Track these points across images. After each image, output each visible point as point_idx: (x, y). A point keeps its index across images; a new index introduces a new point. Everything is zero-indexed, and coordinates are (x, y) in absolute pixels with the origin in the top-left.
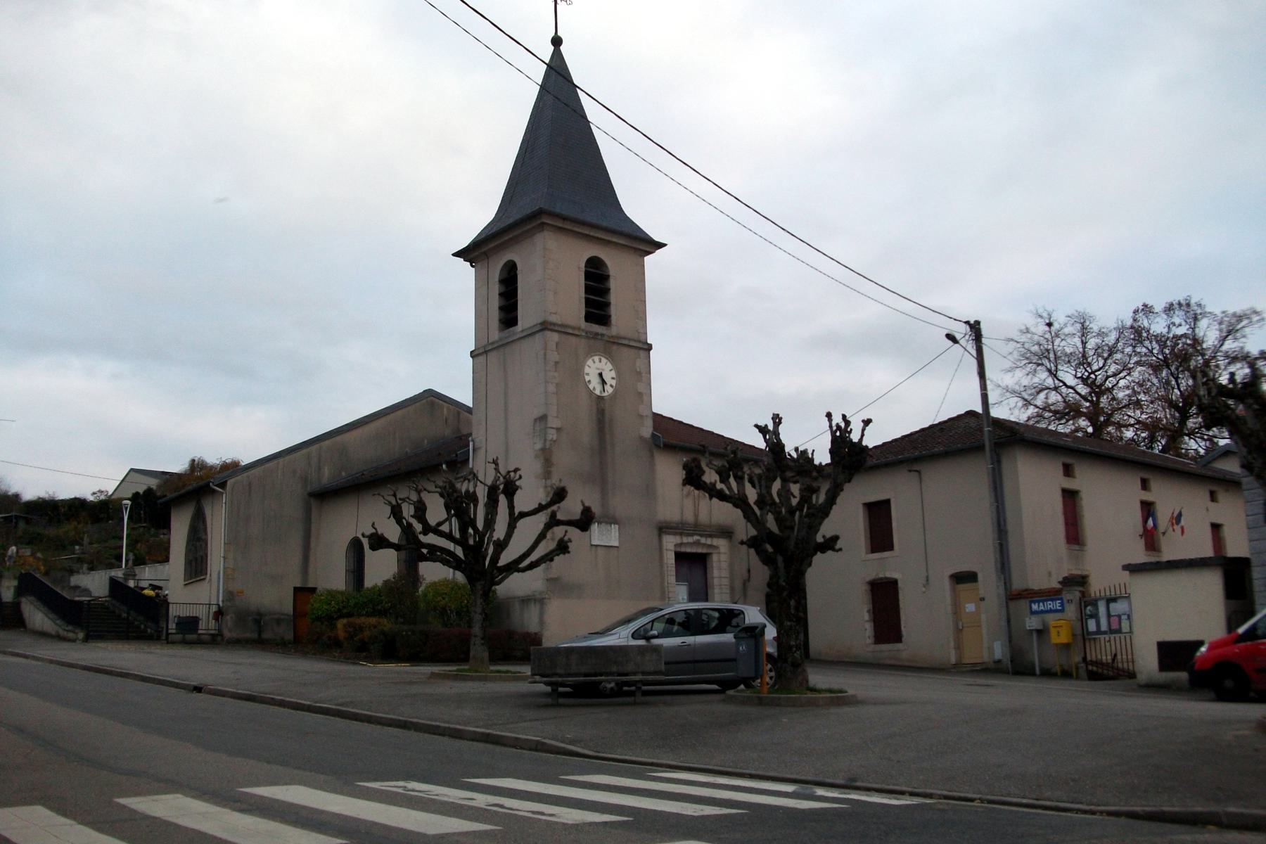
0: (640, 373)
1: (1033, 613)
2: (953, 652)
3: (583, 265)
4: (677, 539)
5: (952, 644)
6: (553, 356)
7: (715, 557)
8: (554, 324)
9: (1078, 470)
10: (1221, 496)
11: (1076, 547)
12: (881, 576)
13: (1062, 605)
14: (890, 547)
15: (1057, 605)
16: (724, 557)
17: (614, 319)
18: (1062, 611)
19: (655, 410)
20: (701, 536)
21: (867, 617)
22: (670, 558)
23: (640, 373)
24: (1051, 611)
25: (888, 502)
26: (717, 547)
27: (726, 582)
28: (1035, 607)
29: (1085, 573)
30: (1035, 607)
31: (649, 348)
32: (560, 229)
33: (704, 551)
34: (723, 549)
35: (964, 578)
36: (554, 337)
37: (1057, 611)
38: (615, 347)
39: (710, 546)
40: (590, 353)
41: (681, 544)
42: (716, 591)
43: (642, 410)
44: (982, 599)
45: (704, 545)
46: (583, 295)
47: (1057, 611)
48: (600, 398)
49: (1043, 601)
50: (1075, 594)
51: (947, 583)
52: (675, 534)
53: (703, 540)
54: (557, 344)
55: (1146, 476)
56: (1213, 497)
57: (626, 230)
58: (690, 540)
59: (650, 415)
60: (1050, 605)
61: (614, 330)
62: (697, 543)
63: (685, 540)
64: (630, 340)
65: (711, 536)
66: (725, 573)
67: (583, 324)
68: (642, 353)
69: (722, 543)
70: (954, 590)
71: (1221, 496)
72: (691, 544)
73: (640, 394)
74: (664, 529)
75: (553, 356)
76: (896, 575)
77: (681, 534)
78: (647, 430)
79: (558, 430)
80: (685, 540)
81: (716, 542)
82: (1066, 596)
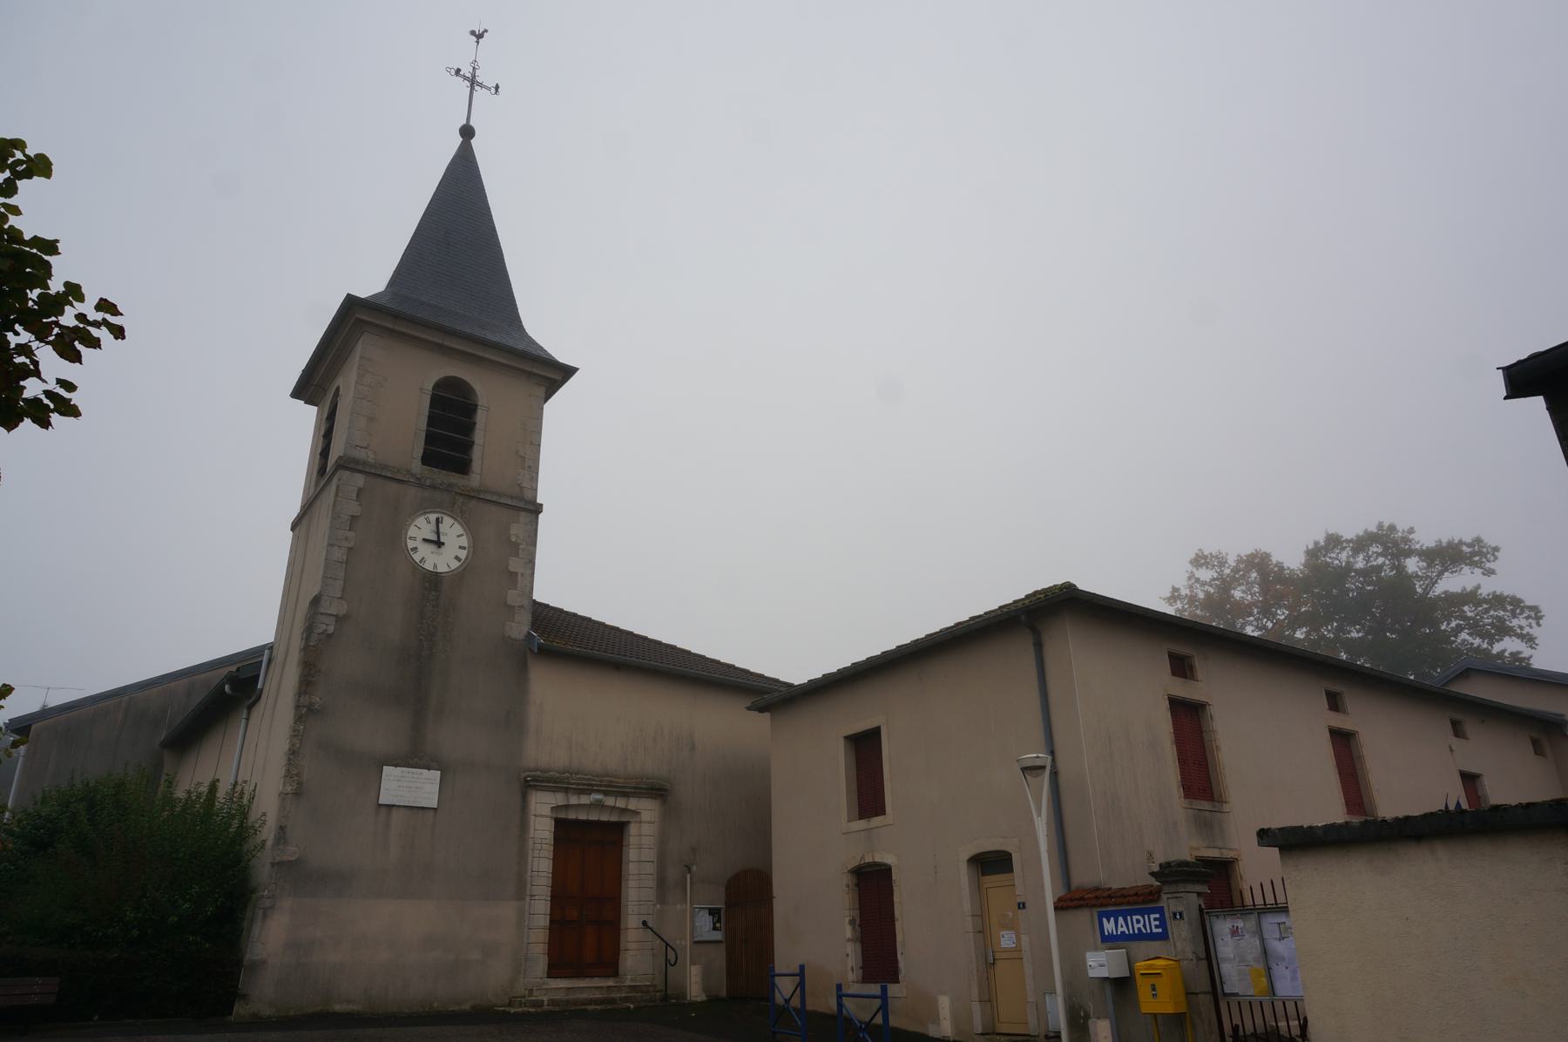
0: (515, 545)
1: (1109, 940)
2: (976, 1008)
3: (429, 386)
4: (560, 799)
5: (975, 992)
6: (354, 508)
7: (633, 829)
8: (365, 463)
9: (1201, 666)
10: (1470, 727)
11: (1206, 805)
12: (868, 859)
13: (1163, 924)
14: (880, 810)
15: (1151, 923)
16: (647, 829)
17: (476, 465)
18: (1164, 936)
19: (542, 594)
20: (606, 793)
21: (849, 932)
22: (542, 830)
23: (515, 545)
24: (1140, 937)
25: (878, 728)
26: (636, 813)
27: (650, 868)
28: (1109, 926)
29: (1228, 854)
30: (1109, 926)
31: (537, 509)
32: (391, 332)
33: (614, 818)
34: (645, 816)
35: (992, 864)
36: (360, 480)
37: (1152, 937)
38: (473, 503)
39: (624, 811)
40: (422, 508)
41: (567, 807)
42: (632, 884)
43: (513, 597)
44: (1022, 906)
45: (613, 808)
46: (424, 426)
47: (1152, 937)
48: (433, 580)
49: (1125, 914)
50: (1187, 900)
51: (964, 874)
52: (554, 790)
53: (610, 801)
54: (360, 491)
55: (1337, 688)
56: (1458, 730)
57: (521, 346)
58: (585, 800)
59: (526, 603)
60: (1138, 923)
61: (474, 480)
62: (599, 805)
63: (574, 800)
64: (500, 495)
65: (625, 795)
66: (650, 854)
67: (416, 466)
68: (523, 517)
69: (648, 809)
70: (979, 892)
71: (1470, 727)
72: (584, 808)
73: (513, 576)
74: (534, 782)
75: (354, 508)
76: (888, 859)
77: (566, 790)
78: (520, 627)
79: (339, 619)
80: (574, 800)
81: (633, 804)
82: (1169, 904)
